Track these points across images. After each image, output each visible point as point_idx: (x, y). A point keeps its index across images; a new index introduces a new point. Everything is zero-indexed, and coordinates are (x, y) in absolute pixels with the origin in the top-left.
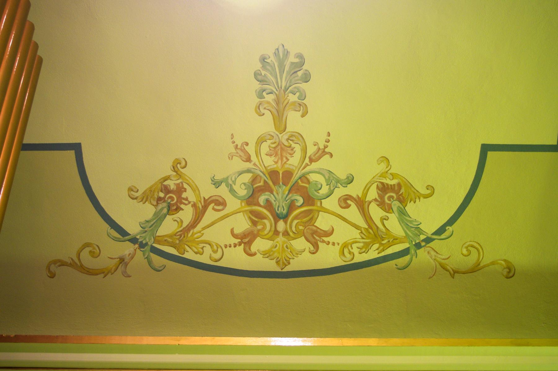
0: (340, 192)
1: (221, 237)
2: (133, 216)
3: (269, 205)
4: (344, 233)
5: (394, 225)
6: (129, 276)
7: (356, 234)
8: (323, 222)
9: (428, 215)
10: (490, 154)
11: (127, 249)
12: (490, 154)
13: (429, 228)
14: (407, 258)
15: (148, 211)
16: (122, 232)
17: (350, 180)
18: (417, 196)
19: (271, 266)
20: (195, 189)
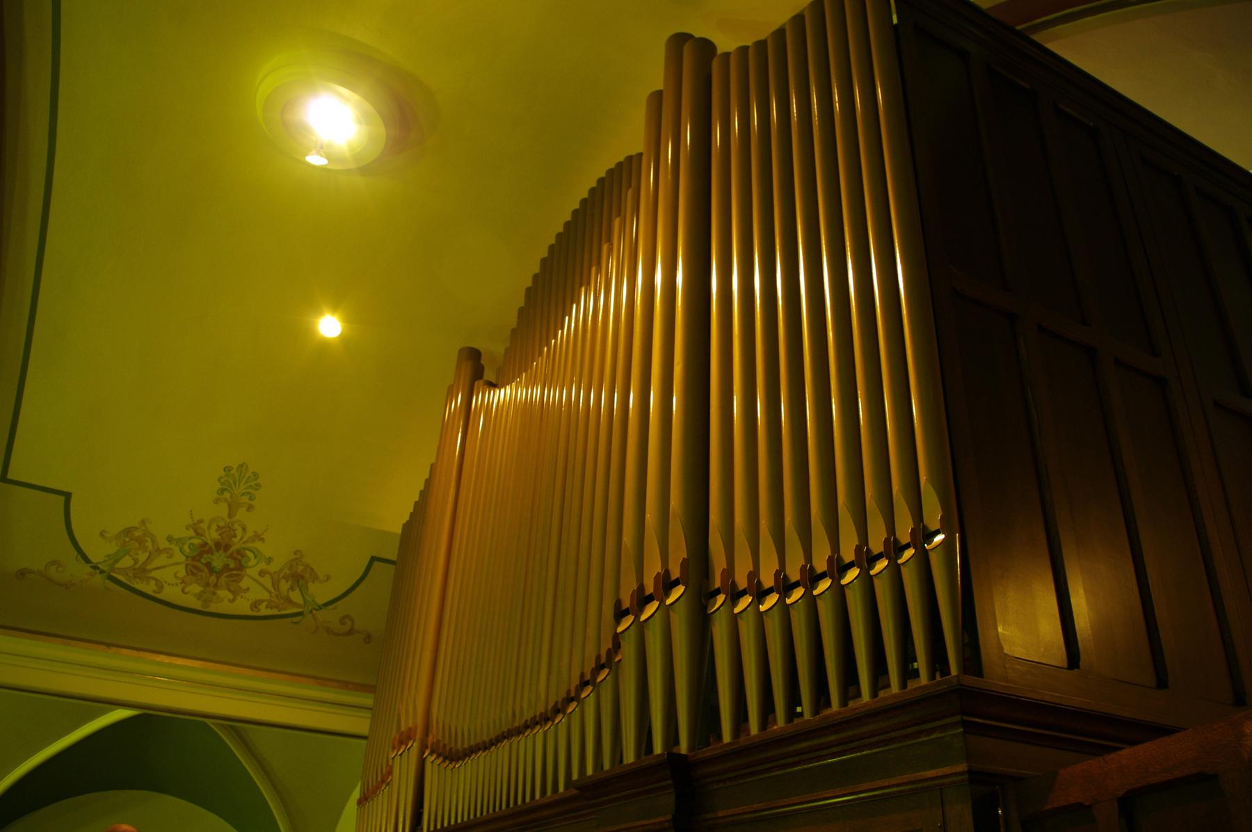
0: (263, 566)
1: (170, 578)
2: (98, 551)
3: (208, 565)
4: (256, 593)
5: (296, 596)
6: (328, 578)
7: (266, 596)
8: (245, 583)
9: (321, 592)
10: (62, 499)
11: (83, 570)
12: (62, 499)
13: (321, 601)
14: (299, 618)
15: (113, 548)
16: (87, 560)
17: (269, 560)
18: (315, 578)
19: (197, 605)
20: (153, 541)
